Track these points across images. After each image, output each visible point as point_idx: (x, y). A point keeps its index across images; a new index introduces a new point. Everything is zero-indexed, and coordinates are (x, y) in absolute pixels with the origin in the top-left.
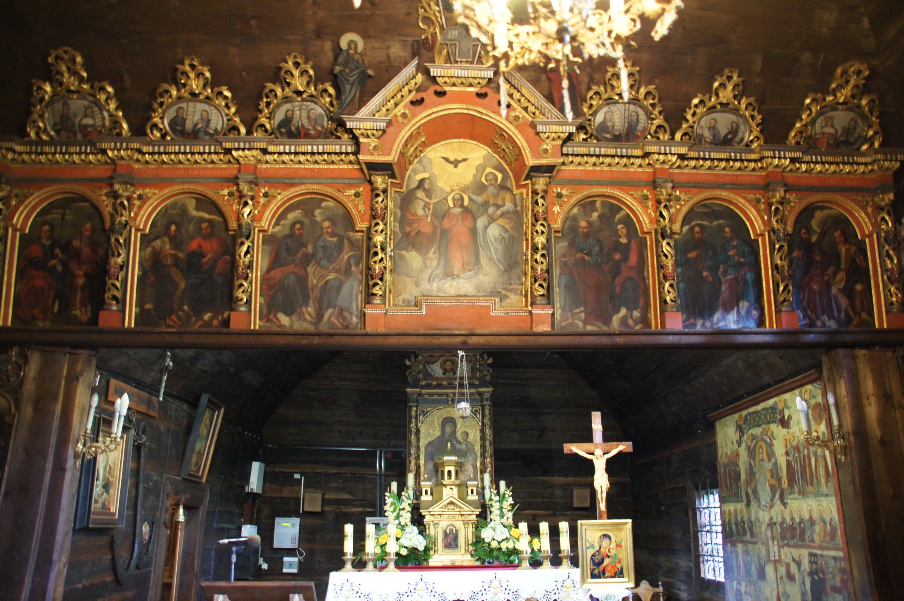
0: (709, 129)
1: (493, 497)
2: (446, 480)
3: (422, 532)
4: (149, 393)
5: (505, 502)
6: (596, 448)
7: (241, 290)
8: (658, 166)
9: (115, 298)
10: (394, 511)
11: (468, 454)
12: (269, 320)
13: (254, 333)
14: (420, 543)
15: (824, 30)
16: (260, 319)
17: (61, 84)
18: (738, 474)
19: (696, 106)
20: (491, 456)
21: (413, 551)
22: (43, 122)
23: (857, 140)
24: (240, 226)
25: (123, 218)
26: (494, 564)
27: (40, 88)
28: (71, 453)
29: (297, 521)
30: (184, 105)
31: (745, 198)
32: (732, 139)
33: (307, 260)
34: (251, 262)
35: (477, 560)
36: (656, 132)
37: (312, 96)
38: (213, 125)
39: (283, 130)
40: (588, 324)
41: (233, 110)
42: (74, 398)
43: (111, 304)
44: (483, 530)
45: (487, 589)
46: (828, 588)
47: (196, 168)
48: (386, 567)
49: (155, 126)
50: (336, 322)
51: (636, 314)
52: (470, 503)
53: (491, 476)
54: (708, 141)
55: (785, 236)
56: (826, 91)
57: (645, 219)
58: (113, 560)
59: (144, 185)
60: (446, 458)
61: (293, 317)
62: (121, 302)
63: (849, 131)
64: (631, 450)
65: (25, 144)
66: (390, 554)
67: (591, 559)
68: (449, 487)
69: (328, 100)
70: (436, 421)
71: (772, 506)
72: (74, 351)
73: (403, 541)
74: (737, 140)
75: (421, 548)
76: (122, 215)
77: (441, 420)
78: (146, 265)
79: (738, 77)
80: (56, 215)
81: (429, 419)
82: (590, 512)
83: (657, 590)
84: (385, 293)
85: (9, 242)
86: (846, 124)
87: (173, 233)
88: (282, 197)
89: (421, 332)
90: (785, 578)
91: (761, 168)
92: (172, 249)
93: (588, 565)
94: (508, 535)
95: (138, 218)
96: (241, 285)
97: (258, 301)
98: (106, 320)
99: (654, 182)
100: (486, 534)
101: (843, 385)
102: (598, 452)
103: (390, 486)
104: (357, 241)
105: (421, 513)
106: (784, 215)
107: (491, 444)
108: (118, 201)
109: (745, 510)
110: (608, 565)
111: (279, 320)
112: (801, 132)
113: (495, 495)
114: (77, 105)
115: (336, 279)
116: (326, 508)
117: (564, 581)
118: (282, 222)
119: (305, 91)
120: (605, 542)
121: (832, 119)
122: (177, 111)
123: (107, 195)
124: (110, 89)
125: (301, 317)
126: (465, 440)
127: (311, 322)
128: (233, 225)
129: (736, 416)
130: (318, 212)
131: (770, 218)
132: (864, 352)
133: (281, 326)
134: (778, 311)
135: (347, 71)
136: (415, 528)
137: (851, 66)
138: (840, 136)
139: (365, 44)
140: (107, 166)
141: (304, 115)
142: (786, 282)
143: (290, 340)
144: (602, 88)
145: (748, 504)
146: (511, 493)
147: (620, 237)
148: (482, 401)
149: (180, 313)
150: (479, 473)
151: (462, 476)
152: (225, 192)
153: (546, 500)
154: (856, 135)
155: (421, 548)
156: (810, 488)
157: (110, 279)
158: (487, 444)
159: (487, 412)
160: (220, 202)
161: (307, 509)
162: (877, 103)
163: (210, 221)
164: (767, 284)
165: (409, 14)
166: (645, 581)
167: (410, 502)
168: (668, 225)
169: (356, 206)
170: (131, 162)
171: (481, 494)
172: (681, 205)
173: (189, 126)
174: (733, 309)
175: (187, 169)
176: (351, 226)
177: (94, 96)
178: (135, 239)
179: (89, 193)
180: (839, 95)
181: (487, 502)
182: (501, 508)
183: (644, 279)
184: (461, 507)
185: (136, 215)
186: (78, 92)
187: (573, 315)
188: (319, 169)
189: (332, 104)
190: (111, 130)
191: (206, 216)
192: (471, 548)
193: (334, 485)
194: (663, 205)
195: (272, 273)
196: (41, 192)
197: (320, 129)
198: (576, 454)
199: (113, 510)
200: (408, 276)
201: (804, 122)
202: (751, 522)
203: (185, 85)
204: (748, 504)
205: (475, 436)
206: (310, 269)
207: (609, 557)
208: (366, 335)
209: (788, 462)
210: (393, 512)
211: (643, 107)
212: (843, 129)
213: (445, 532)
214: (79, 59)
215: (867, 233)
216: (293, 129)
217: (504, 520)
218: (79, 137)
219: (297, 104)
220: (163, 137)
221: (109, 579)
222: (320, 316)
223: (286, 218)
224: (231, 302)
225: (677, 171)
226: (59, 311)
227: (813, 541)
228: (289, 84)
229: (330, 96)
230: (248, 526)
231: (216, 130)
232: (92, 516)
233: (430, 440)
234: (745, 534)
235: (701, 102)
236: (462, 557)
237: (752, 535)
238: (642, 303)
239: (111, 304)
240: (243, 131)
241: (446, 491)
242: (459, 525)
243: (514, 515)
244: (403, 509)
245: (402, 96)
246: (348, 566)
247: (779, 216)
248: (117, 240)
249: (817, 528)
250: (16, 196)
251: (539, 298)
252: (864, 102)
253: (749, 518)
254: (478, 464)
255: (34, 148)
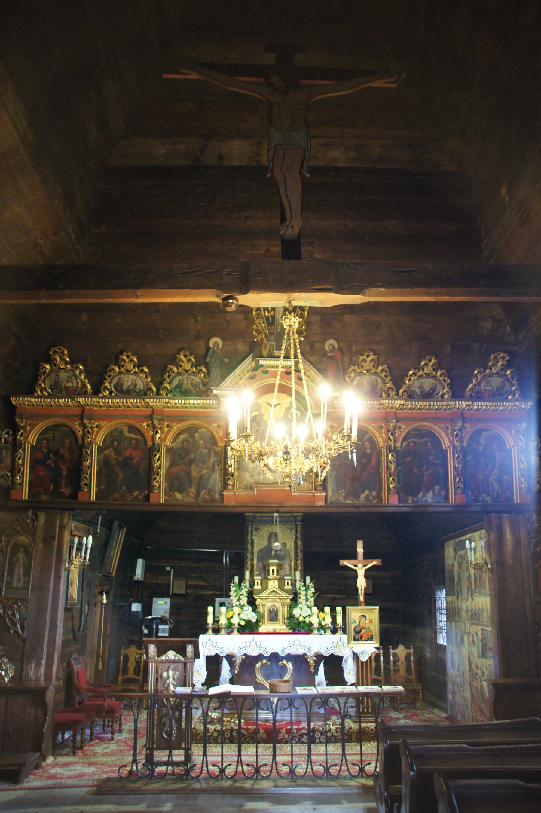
0: (419, 388)
1: (301, 588)
2: (271, 576)
3: (254, 610)
4: (88, 525)
5: (309, 591)
6: (360, 563)
7: (155, 481)
8: (388, 410)
9: (86, 484)
10: (236, 596)
11: (286, 558)
12: (170, 496)
13: (162, 505)
14: (253, 617)
15: (485, 332)
16: (165, 495)
17: (55, 365)
18: (454, 577)
19: (411, 375)
20: (301, 559)
21: (249, 622)
22: (44, 384)
23: (505, 393)
24: (154, 444)
25: (89, 439)
26: (301, 632)
27: (44, 367)
28: (63, 567)
29: (168, 600)
30: (122, 376)
31: (439, 427)
32: (432, 393)
33: (192, 462)
34: (160, 465)
35: (290, 629)
36: (387, 390)
37: (194, 372)
38: (138, 387)
39: (177, 390)
40: (348, 499)
41: (149, 379)
42: (64, 539)
43: (84, 488)
44: (294, 609)
45: (292, 646)
46: (488, 648)
47: (129, 410)
48: (232, 632)
49: (106, 387)
50: (207, 497)
51: (374, 493)
52: (286, 591)
53: (301, 573)
54: (419, 394)
55: (461, 449)
56: (485, 368)
57: (381, 440)
58: (73, 625)
59: (100, 420)
60: (271, 561)
61: (184, 494)
62: (89, 486)
63: (500, 388)
64: (380, 564)
65: (35, 397)
66: (235, 624)
67: (354, 629)
68: (272, 581)
69: (203, 375)
70: (265, 535)
71: (467, 600)
72: (62, 512)
73: (242, 616)
74: (436, 393)
75: (254, 620)
76: (88, 437)
77: (268, 534)
78: (101, 464)
79: (435, 359)
80: (49, 435)
81: (260, 533)
82: (356, 603)
83: (409, 651)
84: (234, 483)
85: (26, 451)
86: (499, 385)
87: (115, 446)
88: (176, 427)
89: (254, 505)
90: (472, 643)
91: (450, 409)
92: (115, 455)
93: (353, 633)
94: (310, 613)
95: (97, 439)
96: (156, 478)
97: (164, 485)
98: (81, 497)
99: (386, 419)
100: (296, 612)
101: (493, 534)
102: (360, 565)
103: (234, 579)
104: (219, 451)
105: (254, 598)
106: (461, 437)
107: (301, 551)
108: (86, 430)
109: (456, 601)
110: (364, 633)
111: (175, 496)
112: (472, 389)
113: (303, 586)
114: (63, 375)
115: (207, 473)
116: (189, 591)
117: (338, 642)
118: (177, 440)
119: (189, 370)
120: (363, 620)
121: (490, 381)
122: (118, 379)
123: (79, 425)
124: (81, 367)
125: (188, 495)
126: (284, 548)
127: (194, 498)
128: (150, 443)
129: (453, 541)
130: (196, 435)
131: (453, 438)
132: (506, 515)
133: (177, 499)
134: (455, 493)
135: (213, 360)
136: (250, 608)
137: (499, 354)
138: (496, 391)
139: (223, 343)
140: (79, 408)
141: (189, 382)
142: (460, 477)
143: (183, 509)
144: (356, 367)
145: (458, 598)
146: (313, 585)
147: (366, 449)
148: (296, 522)
149: (121, 491)
150: (293, 570)
151: (282, 573)
152: (145, 424)
153: (341, 588)
154: (505, 390)
155: (254, 620)
156: (483, 591)
157: (83, 474)
158: (299, 551)
159: (299, 529)
160: (142, 430)
161: (175, 592)
162: (515, 373)
163: (137, 440)
164: (451, 477)
165: (247, 327)
166: (401, 645)
167: (247, 590)
168: (393, 445)
169: (218, 434)
170: (93, 407)
171: (294, 584)
172: (401, 432)
173: (125, 387)
174: (430, 490)
175: (123, 410)
176: (216, 444)
177: (73, 371)
178: (95, 448)
179: (69, 424)
180: (493, 369)
181: (298, 590)
182: (306, 595)
183: (379, 474)
184: (280, 594)
185: (96, 437)
186: (63, 369)
187: (338, 494)
188: (197, 411)
189: (204, 376)
190: (81, 389)
191: (134, 436)
192: (286, 621)
193: (194, 575)
194: (390, 433)
195: (172, 469)
196: (43, 422)
197: (198, 390)
198: (347, 566)
199: (74, 597)
200: (247, 472)
201: (474, 384)
202: (459, 609)
203: (123, 366)
204: (458, 598)
205: (291, 545)
206: (193, 467)
207: (365, 628)
208: (225, 506)
209: (475, 573)
210: (235, 597)
211: (381, 378)
212: (497, 387)
213: (270, 610)
214: (66, 352)
215: (511, 446)
216: (183, 390)
217: (308, 603)
218: (64, 392)
219: (185, 376)
220: (111, 393)
221: (71, 636)
222: (198, 494)
223: (178, 438)
224: (150, 487)
225: (400, 411)
226: (53, 488)
227: (483, 622)
228: (181, 366)
229: (204, 373)
230: (136, 604)
231: (140, 390)
232: (68, 601)
233: (261, 547)
234: (456, 616)
235: (413, 373)
236: (281, 627)
237: (459, 618)
238: (377, 488)
239: (84, 488)
240: (154, 389)
241: (271, 583)
242: (279, 605)
243: (315, 600)
244: (242, 595)
245: (244, 375)
246: (210, 631)
247: (458, 438)
248: (86, 452)
249: (485, 614)
250: (30, 425)
251: (319, 487)
252: (508, 372)
253: (458, 606)
254: (293, 564)
255: (40, 399)
